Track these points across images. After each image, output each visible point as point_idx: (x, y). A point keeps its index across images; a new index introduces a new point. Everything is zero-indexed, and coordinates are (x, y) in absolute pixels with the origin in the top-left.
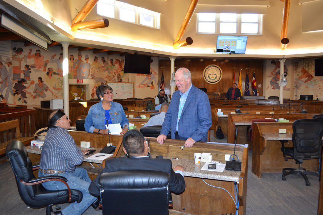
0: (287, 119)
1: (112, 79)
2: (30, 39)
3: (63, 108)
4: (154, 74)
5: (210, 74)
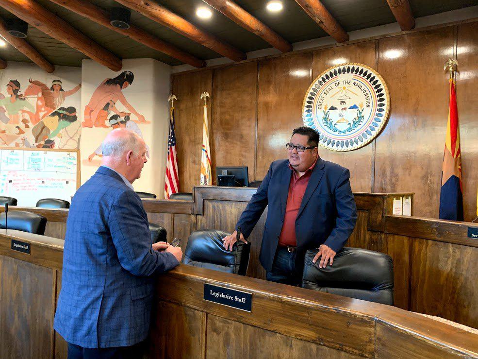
1: (16, 138)
4: (136, 122)
5: (332, 108)
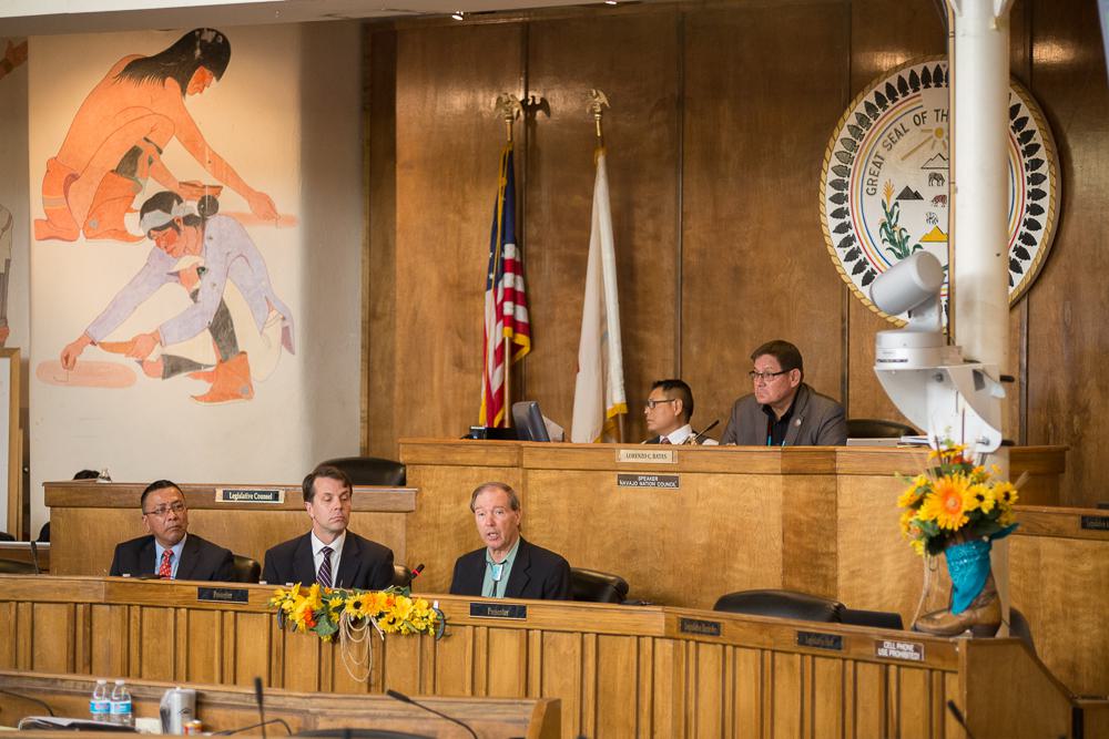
0: (968, 710)
2: (359, 296)
3: (391, 693)
4: (240, 218)
